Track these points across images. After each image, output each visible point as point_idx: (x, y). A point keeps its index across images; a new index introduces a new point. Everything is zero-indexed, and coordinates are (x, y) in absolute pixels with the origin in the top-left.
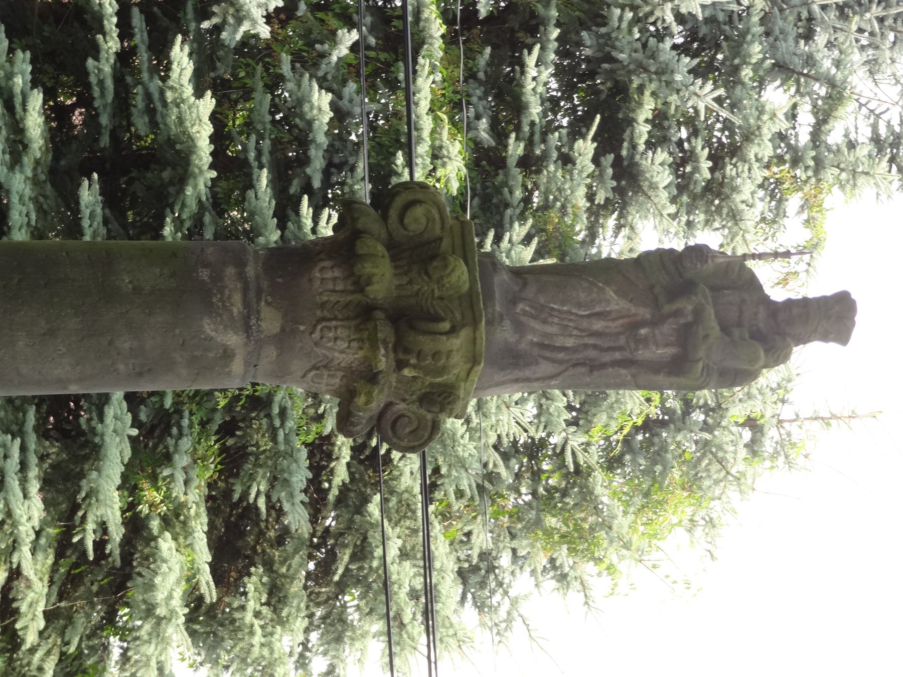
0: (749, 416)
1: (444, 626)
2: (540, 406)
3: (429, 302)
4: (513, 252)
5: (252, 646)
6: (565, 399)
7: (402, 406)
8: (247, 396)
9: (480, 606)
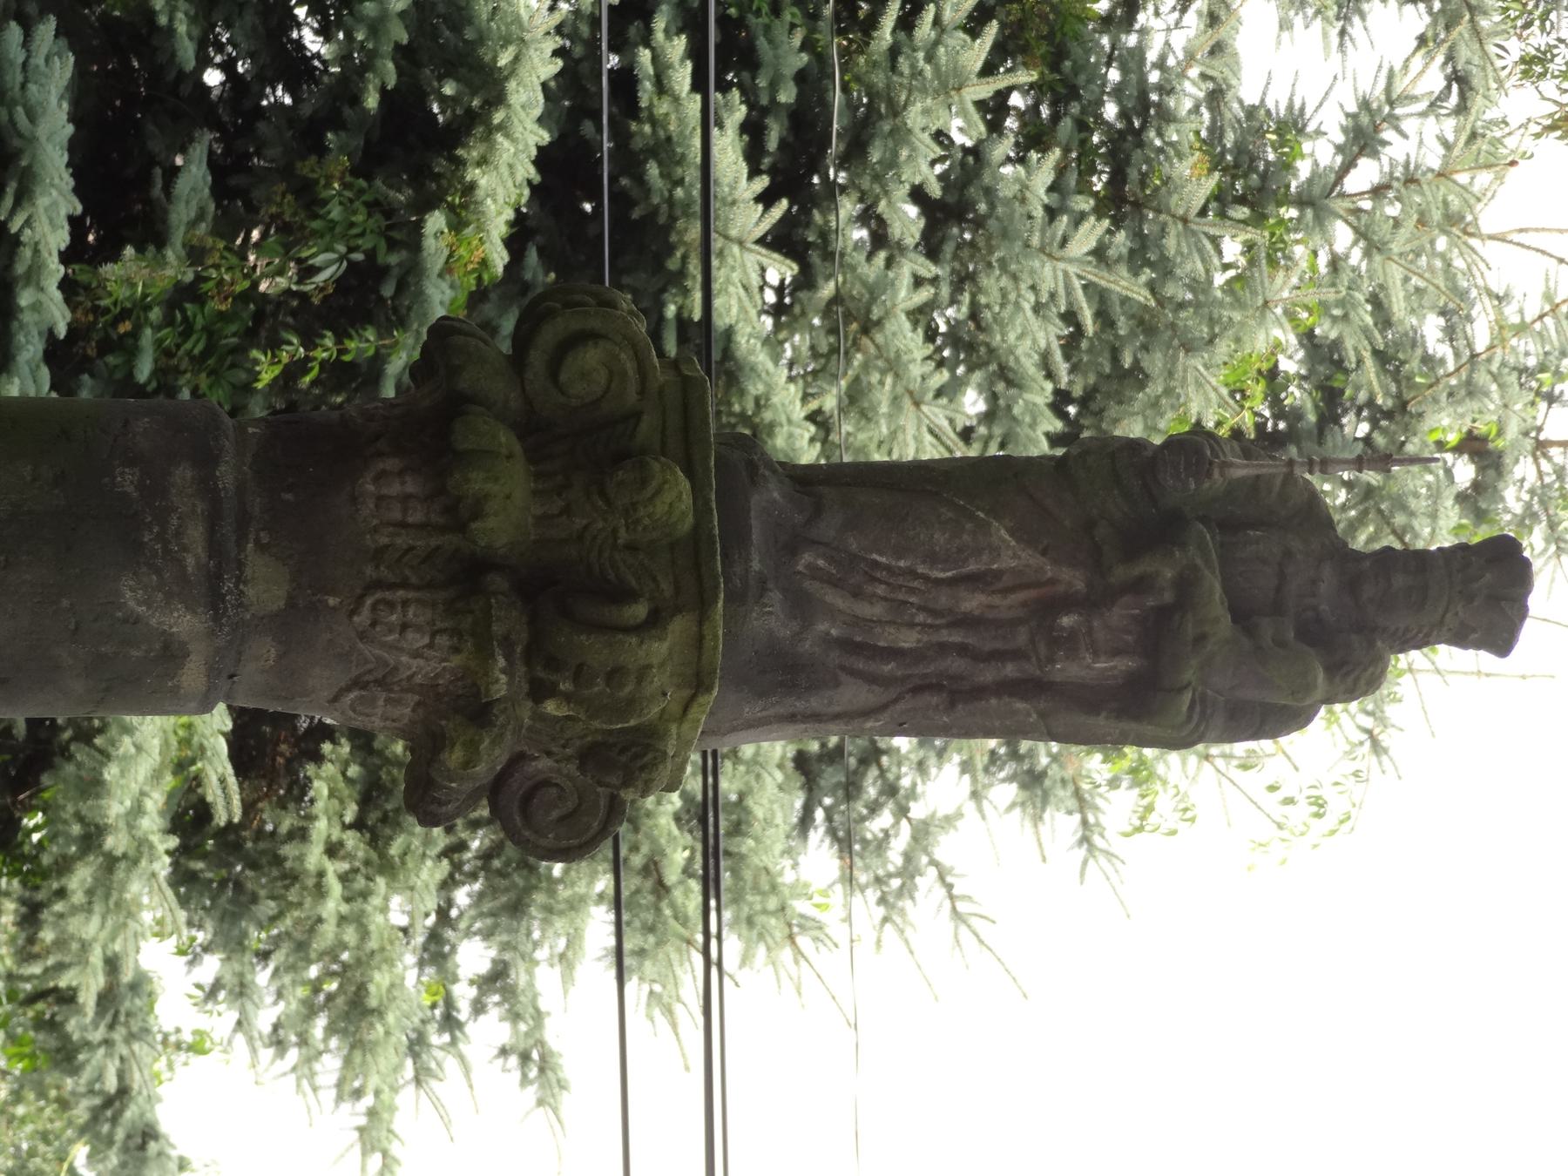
0: (1470, 432)
1: (756, 888)
2: (993, 398)
3: (606, 555)
4: (942, 50)
5: (320, 920)
6: (1049, 386)
7: (544, 764)
8: (323, 363)
9: (844, 840)
